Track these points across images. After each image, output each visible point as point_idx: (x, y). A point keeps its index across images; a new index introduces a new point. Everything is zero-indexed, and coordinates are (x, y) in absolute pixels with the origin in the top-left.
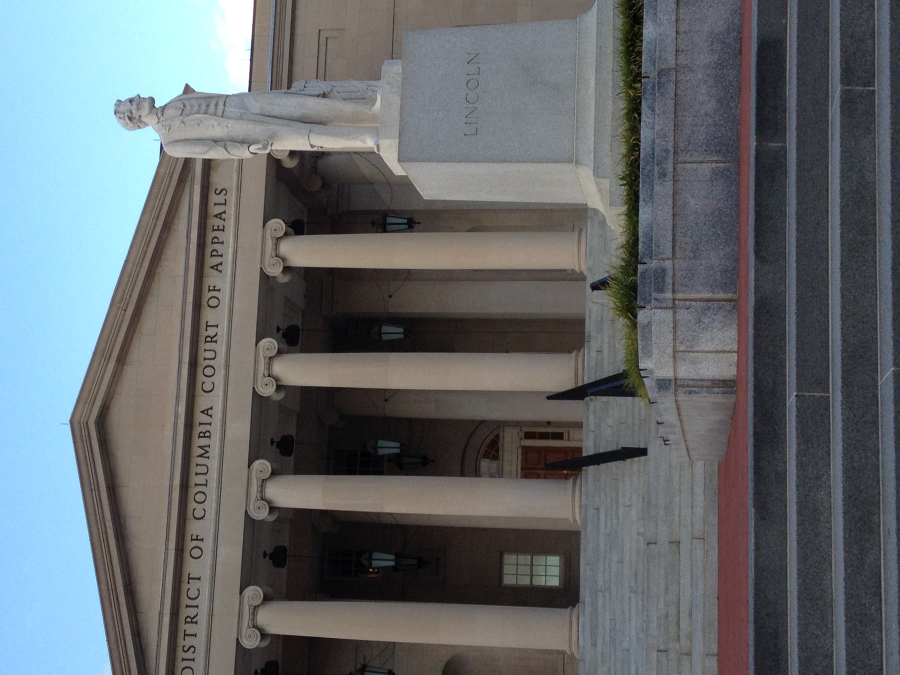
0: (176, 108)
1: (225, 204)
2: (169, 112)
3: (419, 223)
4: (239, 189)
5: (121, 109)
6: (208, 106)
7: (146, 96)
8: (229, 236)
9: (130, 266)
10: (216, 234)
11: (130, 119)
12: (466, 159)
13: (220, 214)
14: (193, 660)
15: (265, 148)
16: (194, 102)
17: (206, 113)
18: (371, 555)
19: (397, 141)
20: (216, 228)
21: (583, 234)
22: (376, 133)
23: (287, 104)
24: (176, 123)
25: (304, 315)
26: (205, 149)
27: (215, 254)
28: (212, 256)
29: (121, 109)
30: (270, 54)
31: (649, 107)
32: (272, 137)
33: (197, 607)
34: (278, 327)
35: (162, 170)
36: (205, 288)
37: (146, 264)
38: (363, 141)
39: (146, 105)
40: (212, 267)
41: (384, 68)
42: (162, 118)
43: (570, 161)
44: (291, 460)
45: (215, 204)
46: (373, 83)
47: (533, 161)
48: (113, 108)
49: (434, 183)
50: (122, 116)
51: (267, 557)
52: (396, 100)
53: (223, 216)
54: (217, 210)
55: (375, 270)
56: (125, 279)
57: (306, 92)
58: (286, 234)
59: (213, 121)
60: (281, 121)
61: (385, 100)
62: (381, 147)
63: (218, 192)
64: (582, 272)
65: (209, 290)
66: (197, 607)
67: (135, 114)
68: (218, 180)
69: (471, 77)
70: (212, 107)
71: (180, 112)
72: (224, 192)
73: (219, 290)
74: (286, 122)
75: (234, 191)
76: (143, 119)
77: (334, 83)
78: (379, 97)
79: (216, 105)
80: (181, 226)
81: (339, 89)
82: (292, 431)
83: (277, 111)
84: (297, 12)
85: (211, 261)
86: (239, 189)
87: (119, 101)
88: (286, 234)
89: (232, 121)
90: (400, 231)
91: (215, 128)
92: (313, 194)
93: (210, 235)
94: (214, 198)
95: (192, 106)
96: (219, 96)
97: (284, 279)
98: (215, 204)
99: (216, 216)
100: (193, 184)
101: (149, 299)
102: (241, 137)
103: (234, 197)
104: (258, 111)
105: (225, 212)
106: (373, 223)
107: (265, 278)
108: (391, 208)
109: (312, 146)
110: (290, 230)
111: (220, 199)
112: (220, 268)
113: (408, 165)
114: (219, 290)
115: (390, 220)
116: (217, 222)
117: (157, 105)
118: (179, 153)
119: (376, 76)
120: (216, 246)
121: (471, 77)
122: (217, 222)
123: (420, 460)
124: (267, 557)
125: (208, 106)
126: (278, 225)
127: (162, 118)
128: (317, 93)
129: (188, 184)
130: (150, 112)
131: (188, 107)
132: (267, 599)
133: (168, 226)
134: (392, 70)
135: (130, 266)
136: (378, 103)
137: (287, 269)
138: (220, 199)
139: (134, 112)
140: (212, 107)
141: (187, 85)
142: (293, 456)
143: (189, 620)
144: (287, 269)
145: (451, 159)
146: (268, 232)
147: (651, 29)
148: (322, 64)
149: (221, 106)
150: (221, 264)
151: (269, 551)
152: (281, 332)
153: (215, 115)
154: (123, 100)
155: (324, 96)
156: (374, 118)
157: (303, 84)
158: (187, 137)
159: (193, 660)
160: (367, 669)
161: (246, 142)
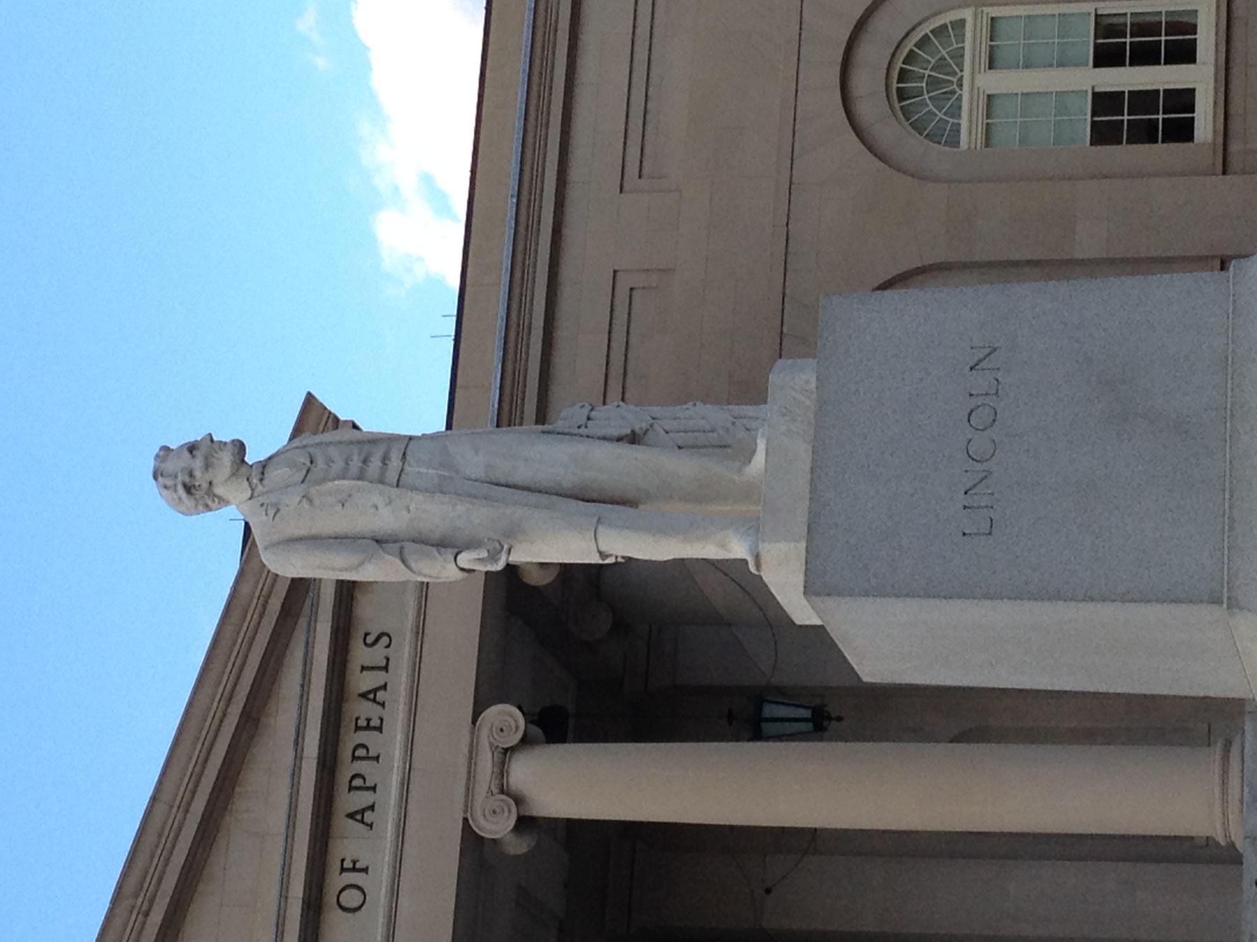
0: (293, 465)
1: (386, 668)
2: (277, 474)
3: (839, 719)
4: (420, 631)
5: (170, 466)
6: (365, 461)
7: (227, 438)
8: (392, 744)
9: (161, 808)
10: (362, 737)
11: (189, 489)
12: (966, 592)
13: (375, 691)
15: (493, 557)
16: (333, 452)
17: (360, 477)
19: (803, 544)
20: (362, 723)
21: (1235, 750)
22: (754, 528)
23: (542, 456)
24: (292, 500)
26: (354, 559)
27: (358, 784)
28: (351, 788)
29: (170, 466)
30: (500, 324)
32: (513, 532)
35: (245, 589)
36: (335, 866)
37: (199, 806)
38: (723, 546)
39: (226, 458)
40: (351, 816)
41: (774, 378)
42: (260, 488)
43: (1216, 601)
45: (363, 668)
46: (750, 410)
47: (1126, 598)
48: (151, 464)
49: (883, 643)
50: (169, 482)
52: (802, 452)
53: (380, 695)
54: (367, 681)
55: (732, 828)
56: (151, 838)
57: (593, 429)
58: (526, 741)
59: (376, 496)
60: (533, 498)
61: (774, 448)
62: (766, 559)
63: (370, 640)
64: (1232, 845)
65: (343, 870)
67: (200, 478)
68: (369, 615)
69: (980, 401)
70: (375, 463)
71: (299, 476)
72: (385, 640)
73: (365, 870)
74: (544, 499)
75: (409, 636)
76: (219, 490)
77: (656, 410)
78: (761, 446)
79: (385, 460)
80: (282, 719)
81: (668, 424)
83: (523, 474)
84: (566, 231)
85: (349, 801)
86: (420, 631)
87: (166, 449)
88: (526, 741)
89: (419, 497)
90: (791, 737)
91: (381, 512)
92: (591, 653)
93: (351, 739)
94: (361, 654)
95: (329, 461)
96: (392, 439)
97: (519, 847)
98: (363, 668)
99: (364, 696)
100: (312, 621)
101: (201, 887)
102: (436, 536)
103: (407, 651)
104: (480, 473)
105: (384, 687)
106: (731, 716)
107: (472, 842)
108: (774, 681)
109: (603, 555)
110: (536, 731)
111: (375, 655)
112: (368, 816)
113: (831, 603)
114: (365, 870)
115: (770, 710)
116: (366, 710)
117: (249, 459)
118: (289, 566)
119: (751, 390)
120: (360, 767)
121: (980, 401)
122: (366, 710)
125: (365, 461)
126: (506, 719)
127: (260, 488)
128: (616, 432)
129: (303, 622)
130: (234, 474)
131: (320, 461)
133: (252, 719)
134: (794, 382)
135: (161, 808)
136: (759, 459)
137: (526, 823)
138: (375, 655)
139: (198, 474)
140: (375, 463)
141: (310, 400)
144: (526, 823)
145: (931, 592)
146: (485, 732)
148: (618, 347)
149: (395, 462)
150: (372, 808)
153: (381, 482)
154: (174, 446)
155: (633, 439)
156: (749, 493)
157: (585, 411)
158: (314, 531)
161: (448, 544)
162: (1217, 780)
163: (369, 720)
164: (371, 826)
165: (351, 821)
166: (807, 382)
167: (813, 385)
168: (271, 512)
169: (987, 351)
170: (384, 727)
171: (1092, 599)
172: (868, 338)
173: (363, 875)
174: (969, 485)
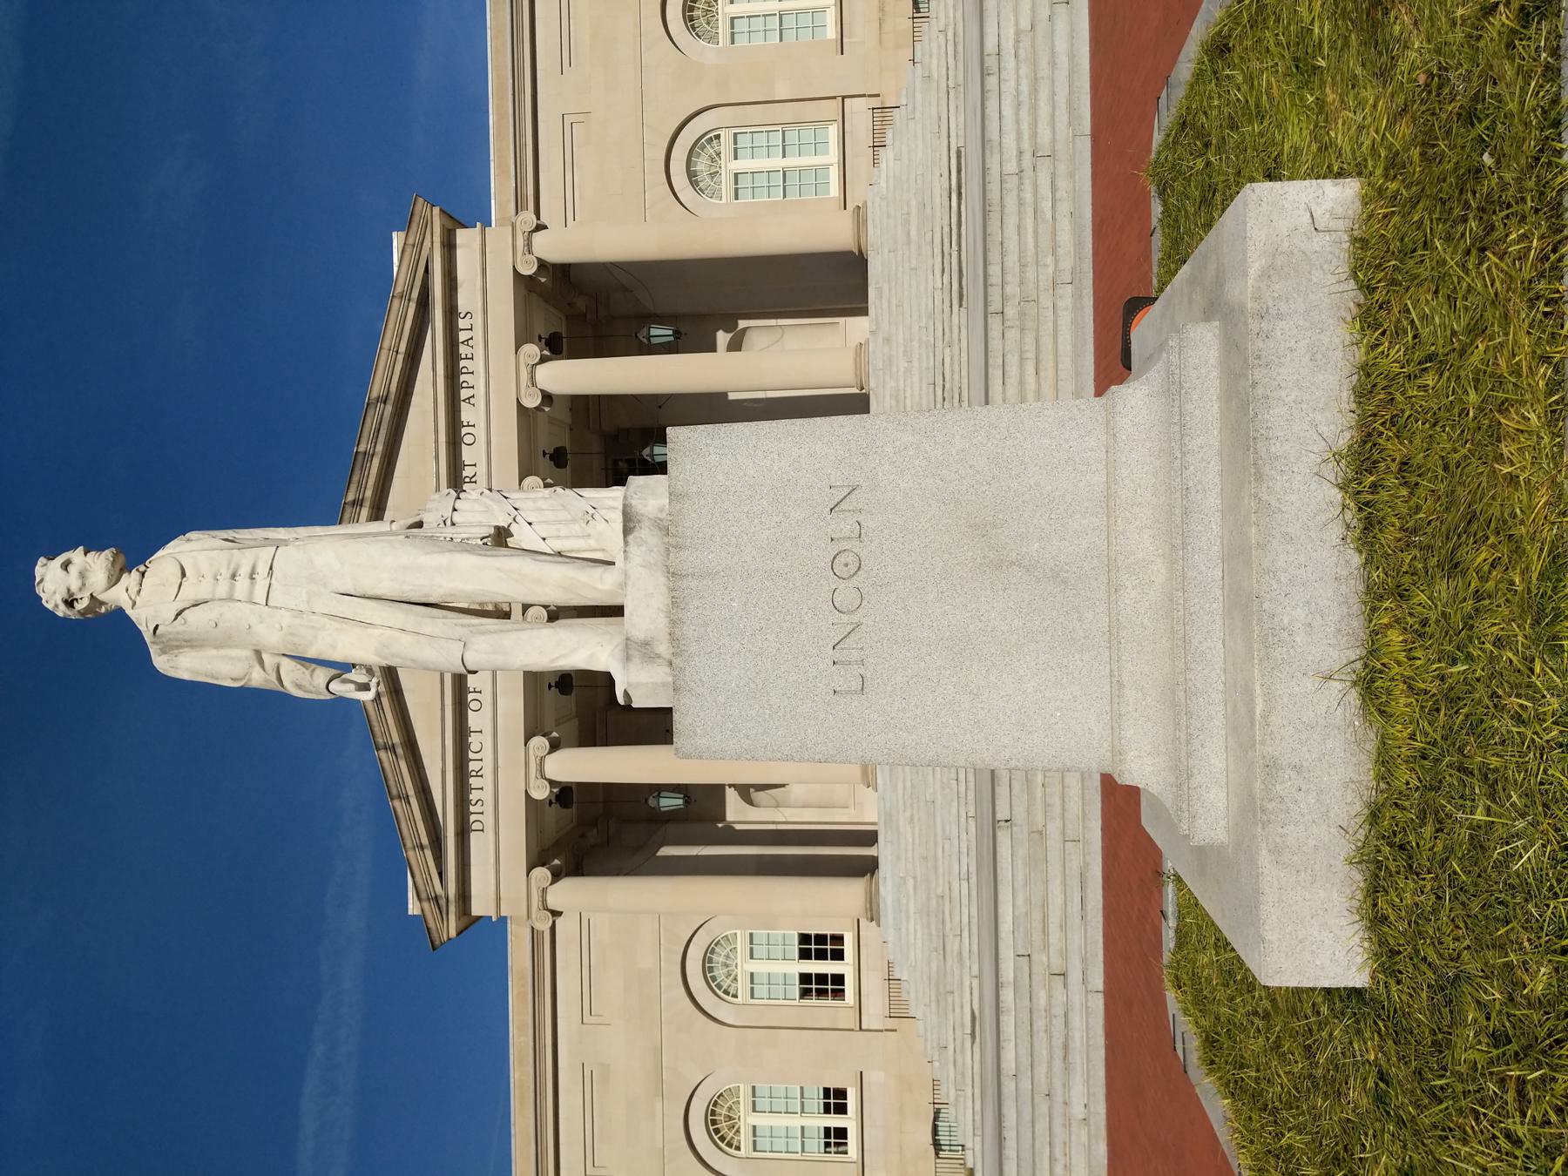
58: (543, 360)
82: (564, 440)
94: (462, 324)
126: (532, 350)
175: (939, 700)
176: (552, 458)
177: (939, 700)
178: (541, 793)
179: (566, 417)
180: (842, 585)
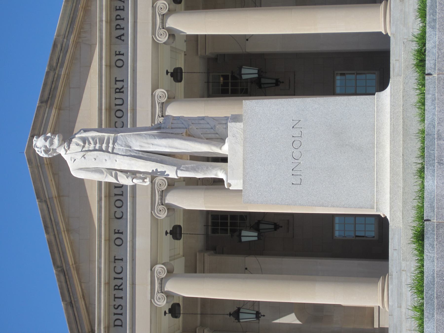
10: (119, 12)
14: (121, 314)
18: (240, 233)
19: (242, 181)
25: (185, 55)
31: (430, 244)
33: (122, 279)
34: (167, 71)
40: (117, 38)
44: (181, 86)
51: (169, 235)
66: (122, 279)
70: (104, 146)
82: (180, 64)
107: (155, 44)
112: (123, 38)
120: (119, 22)
123: (272, 226)
124: (169, 235)
132: (170, 272)
142: (182, 240)
143: (118, 90)
147: (431, 182)
151: (171, 70)
152: (169, 74)
159: (121, 314)
160: (242, 310)
162: (382, 19)
163: (120, 7)
164: (123, 40)
165: (117, 39)
166: (241, 126)
167: (242, 127)
168: (73, 160)
169: (297, 121)
170: (125, 9)
171: (334, 207)
172: (259, 116)
173: (122, 56)
174: (293, 167)
175: (324, 186)
176: (172, 75)
177: (324, 186)
178: (163, 303)
179: (182, 46)
180: (295, 151)
